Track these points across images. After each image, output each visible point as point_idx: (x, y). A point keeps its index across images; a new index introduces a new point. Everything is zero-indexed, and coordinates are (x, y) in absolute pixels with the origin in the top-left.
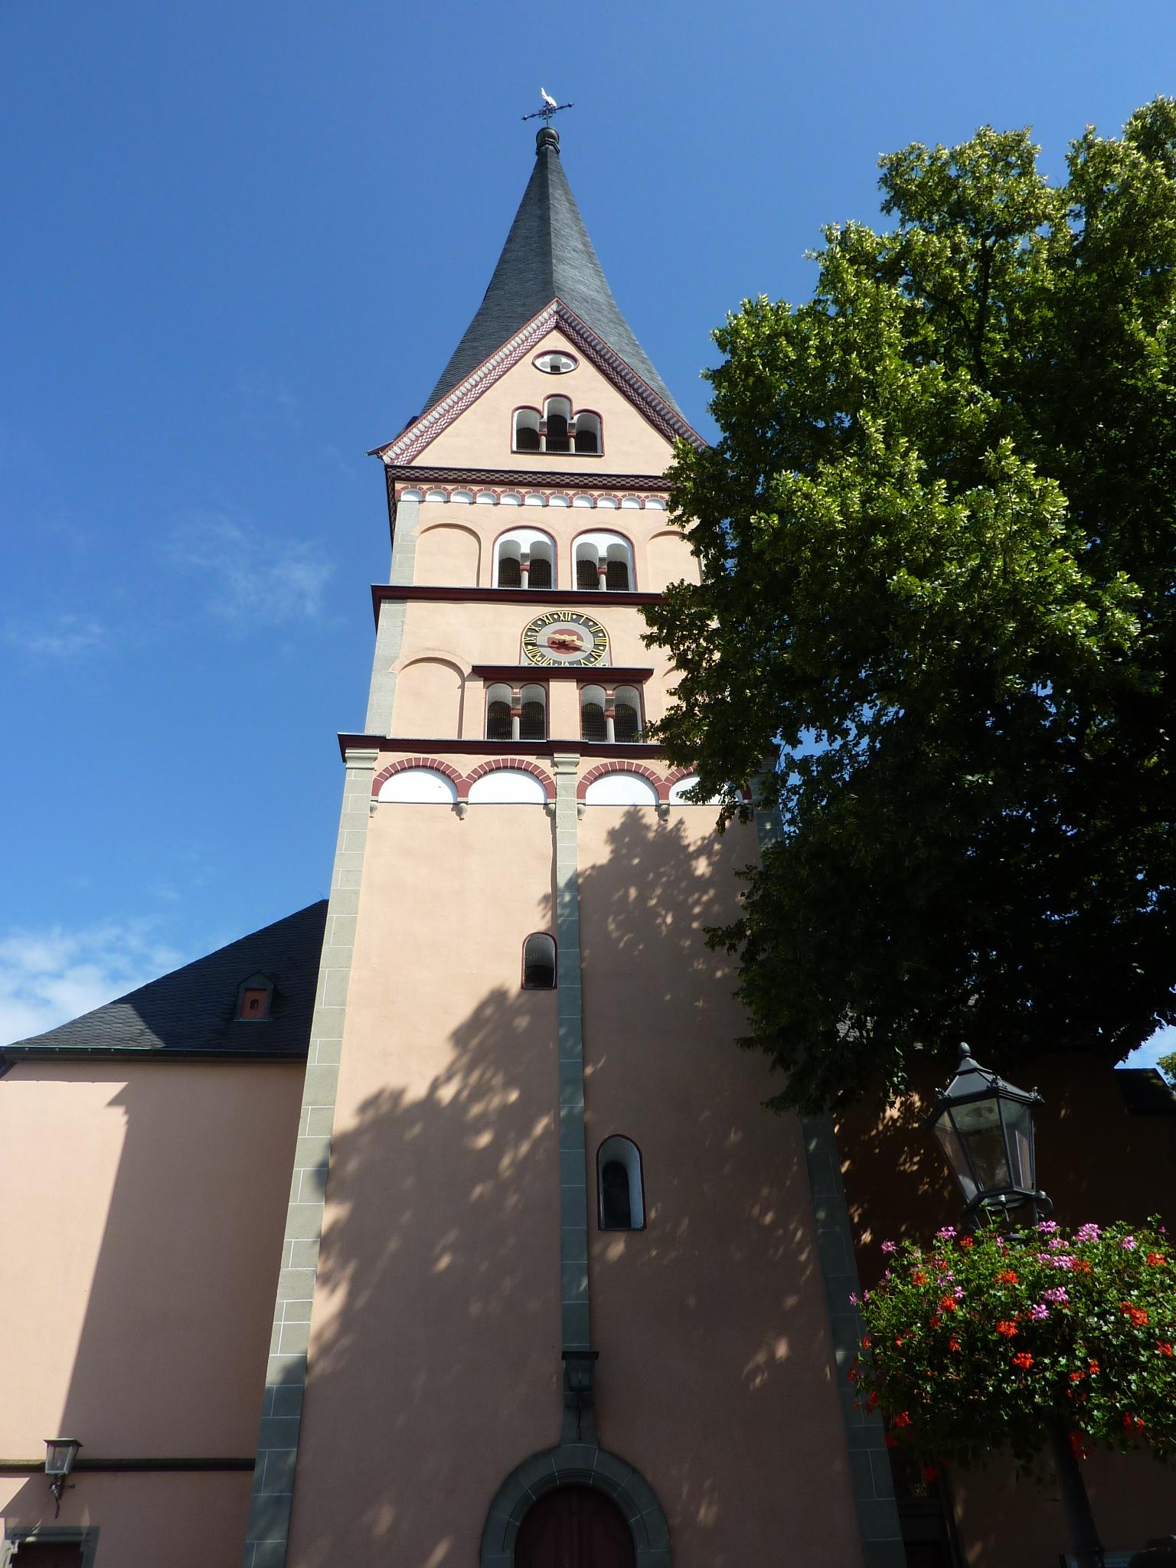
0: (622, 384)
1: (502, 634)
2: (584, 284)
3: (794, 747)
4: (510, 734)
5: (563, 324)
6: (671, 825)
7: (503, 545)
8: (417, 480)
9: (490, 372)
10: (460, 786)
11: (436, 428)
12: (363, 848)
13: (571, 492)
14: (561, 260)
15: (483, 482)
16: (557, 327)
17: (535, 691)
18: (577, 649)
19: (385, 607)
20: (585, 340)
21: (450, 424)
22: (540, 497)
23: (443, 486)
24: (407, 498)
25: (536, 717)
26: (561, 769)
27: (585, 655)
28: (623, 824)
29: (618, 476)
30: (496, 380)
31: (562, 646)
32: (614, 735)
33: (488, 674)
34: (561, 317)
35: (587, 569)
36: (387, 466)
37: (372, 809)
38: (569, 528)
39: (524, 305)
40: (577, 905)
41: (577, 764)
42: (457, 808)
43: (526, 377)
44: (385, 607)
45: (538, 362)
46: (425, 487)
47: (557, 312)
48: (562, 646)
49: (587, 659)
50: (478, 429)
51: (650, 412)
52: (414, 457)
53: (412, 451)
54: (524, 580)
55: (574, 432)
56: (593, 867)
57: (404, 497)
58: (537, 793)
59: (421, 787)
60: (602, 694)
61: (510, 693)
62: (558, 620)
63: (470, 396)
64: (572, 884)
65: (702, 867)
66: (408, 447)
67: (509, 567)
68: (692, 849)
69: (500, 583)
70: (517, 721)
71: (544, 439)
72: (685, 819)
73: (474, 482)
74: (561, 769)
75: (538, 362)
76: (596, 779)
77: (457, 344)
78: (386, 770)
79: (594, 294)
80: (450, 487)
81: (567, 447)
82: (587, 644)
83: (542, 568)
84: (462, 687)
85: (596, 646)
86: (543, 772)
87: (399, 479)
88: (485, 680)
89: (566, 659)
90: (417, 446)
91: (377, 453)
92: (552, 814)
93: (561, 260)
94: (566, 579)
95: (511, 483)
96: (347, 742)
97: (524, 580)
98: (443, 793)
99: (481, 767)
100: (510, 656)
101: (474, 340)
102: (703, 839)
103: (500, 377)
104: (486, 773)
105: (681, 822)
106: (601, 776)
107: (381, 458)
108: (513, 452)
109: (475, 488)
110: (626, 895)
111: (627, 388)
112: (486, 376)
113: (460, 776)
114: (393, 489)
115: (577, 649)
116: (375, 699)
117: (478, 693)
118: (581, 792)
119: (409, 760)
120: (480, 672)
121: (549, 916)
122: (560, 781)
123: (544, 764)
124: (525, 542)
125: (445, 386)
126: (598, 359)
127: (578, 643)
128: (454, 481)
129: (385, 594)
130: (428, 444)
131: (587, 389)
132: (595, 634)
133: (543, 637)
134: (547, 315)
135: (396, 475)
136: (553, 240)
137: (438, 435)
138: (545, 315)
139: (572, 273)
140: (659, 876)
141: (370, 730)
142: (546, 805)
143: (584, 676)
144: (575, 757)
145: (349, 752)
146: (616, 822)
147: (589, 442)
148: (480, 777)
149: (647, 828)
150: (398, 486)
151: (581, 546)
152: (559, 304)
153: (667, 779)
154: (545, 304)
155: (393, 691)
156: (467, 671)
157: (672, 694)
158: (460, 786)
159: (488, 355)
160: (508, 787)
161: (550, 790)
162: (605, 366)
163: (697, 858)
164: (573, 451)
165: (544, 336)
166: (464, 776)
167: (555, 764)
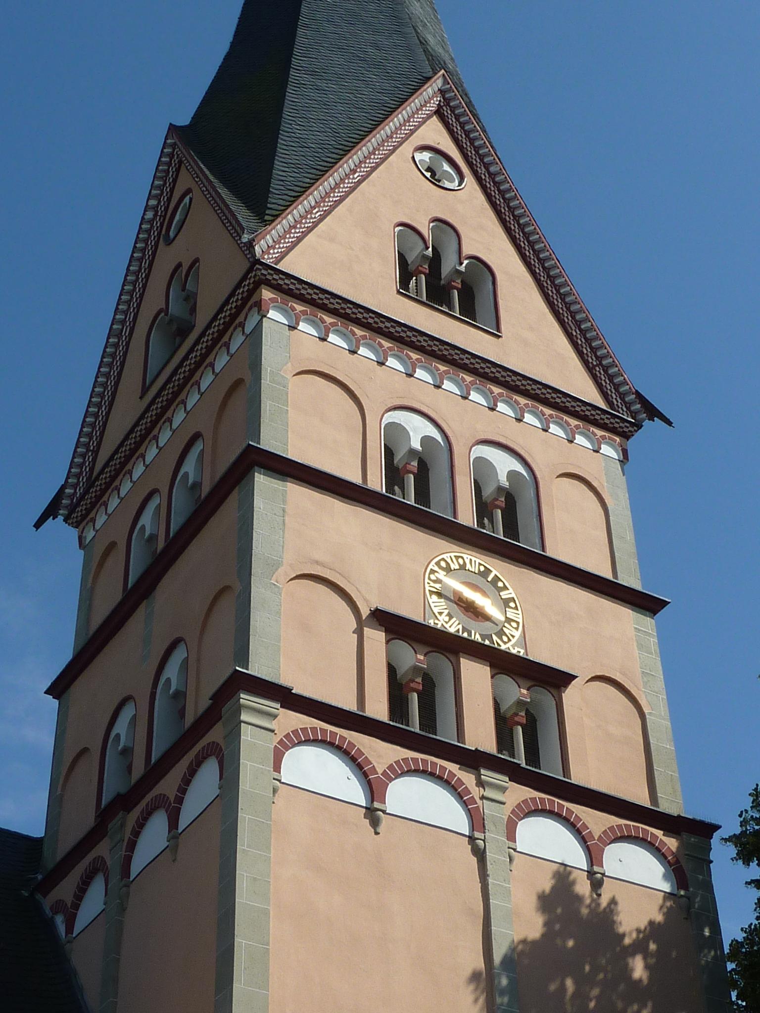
5: (447, 111)
6: (604, 901)
12: (268, 848)
15: (312, 303)
16: (438, 113)
17: (443, 663)
22: (284, 312)
23: (516, 397)
26: (489, 793)
31: (470, 609)
34: (447, 101)
40: (513, 989)
42: (373, 815)
45: (418, 156)
47: (442, 92)
56: (524, 941)
58: (460, 821)
64: (509, 961)
65: (638, 969)
68: (627, 941)
72: (619, 899)
74: (489, 793)
81: (450, 307)
88: (491, 666)
92: (480, 854)
98: (356, 794)
99: (304, 730)
102: (638, 931)
105: (613, 902)
110: (563, 988)
121: (482, 1000)
122: (488, 809)
123: (468, 779)
131: (484, 237)
140: (595, 969)
146: (546, 884)
149: (579, 899)
151: (390, 426)
152: (445, 82)
160: (417, 799)
161: (476, 820)
162: (499, 201)
163: (633, 955)
166: (380, 771)
167: (481, 784)
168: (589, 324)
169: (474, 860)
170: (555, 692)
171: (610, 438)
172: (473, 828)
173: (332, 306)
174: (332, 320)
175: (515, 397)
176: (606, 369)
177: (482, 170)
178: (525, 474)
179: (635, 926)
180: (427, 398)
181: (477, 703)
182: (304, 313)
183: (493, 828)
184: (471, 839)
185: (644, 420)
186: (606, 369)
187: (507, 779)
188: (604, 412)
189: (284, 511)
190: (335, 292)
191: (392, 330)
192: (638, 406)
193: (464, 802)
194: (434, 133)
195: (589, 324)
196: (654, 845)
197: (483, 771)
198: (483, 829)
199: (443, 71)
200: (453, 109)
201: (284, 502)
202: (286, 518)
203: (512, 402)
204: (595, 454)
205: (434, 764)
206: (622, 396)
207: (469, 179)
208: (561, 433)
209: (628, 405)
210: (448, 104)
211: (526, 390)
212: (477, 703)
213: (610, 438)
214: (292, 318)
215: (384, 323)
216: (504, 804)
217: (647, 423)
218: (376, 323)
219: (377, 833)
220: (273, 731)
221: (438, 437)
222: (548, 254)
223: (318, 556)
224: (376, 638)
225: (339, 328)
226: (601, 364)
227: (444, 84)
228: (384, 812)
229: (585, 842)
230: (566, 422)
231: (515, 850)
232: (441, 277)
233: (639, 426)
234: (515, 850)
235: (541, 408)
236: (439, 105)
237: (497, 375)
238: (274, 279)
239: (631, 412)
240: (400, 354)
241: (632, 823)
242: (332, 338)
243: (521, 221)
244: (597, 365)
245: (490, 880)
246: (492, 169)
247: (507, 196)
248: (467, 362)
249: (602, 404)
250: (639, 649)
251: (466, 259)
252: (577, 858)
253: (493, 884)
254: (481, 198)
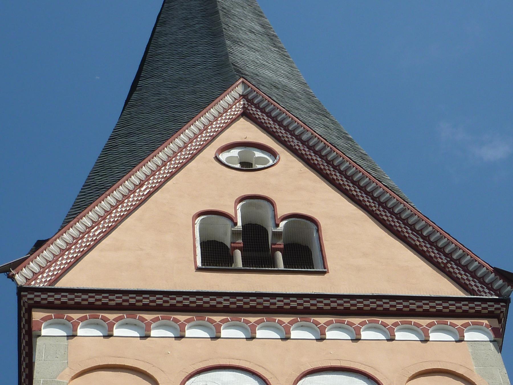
2: (269, 69)
9: (159, 168)
13: (286, 319)
14: (237, 42)
15: (158, 309)
16: (245, 114)
21: (106, 234)
22: (96, 325)
23: (102, 314)
24: (49, 332)
29: (366, 297)
30: (167, 179)
34: (250, 102)
36: (21, 289)
39: (194, 92)
43: (202, 178)
45: (223, 157)
46: (76, 316)
47: (243, 96)
51: (386, 216)
52: (59, 278)
55: (280, 244)
71: (238, 254)
73: (147, 308)
75: (223, 157)
79: (285, 81)
80: (111, 316)
81: (272, 262)
87: (39, 306)
91: (8, 270)
93: (237, 42)
95: (199, 310)
101: (129, 135)
103: (173, 175)
108: (198, 269)
109: (148, 317)
131: (294, 188)
134: (231, 98)
135: (33, 301)
136: (223, 19)
137: (90, 248)
139: (253, 56)
147: (302, 250)
150: (37, 315)
152: (246, 86)
154: (225, 87)
159: (153, 148)
164: (281, 267)
165: (228, 125)
168: (430, 229)
171: (474, 324)
175: (277, 318)
176: (457, 262)
182: (291, 323)
186: (457, 262)
188: (458, 300)
191: (186, 302)
192: (501, 282)
194: (245, 131)
199: (242, 80)
203: (99, 321)
206: (481, 280)
208: (412, 337)
209: (490, 287)
210: (253, 103)
213: (474, 324)
215: (174, 299)
218: (165, 302)
222: (374, 184)
225: (126, 320)
226: (452, 260)
227: (245, 89)
230: (416, 324)
232: (257, 241)
233: (507, 301)
235: (381, 320)
236: (243, 108)
237: (320, 305)
238: (43, 299)
240: (201, 322)
244: (448, 262)
246: (304, 137)
249: (459, 293)
251: (283, 219)
254: (298, 165)
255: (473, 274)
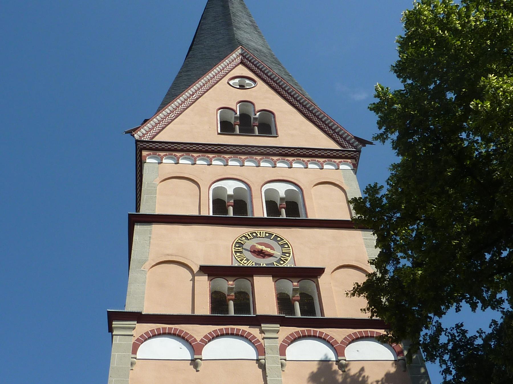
0: (286, 95)
1: (220, 245)
2: (254, 42)
3: (440, 317)
4: (227, 311)
7: (215, 190)
8: (157, 149)
9: (201, 87)
10: (195, 348)
11: (168, 119)
13: (259, 158)
14: (238, 29)
16: (242, 63)
17: (244, 283)
18: (270, 255)
19: (137, 228)
20: (261, 70)
21: (177, 117)
23: (287, 158)
25: (244, 301)
26: (267, 335)
27: (276, 259)
28: (319, 369)
30: (205, 92)
31: (261, 254)
32: (302, 313)
33: (211, 271)
34: (244, 57)
35: (272, 206)
36: (137, 141)
37: (132, 364)
38: (260, 180)
39: (218, 52)
41: (278, 331)
42: (194, 363)
43: (223, 91)
44: (137, 228)
45: (231, 82)
47: (241, 54)
48: (261, 254)
49: (278, 262)
50: (197, 119)
53: (153, 132)
54: (230, 212)
55: (257, 123)
57: (148, 161)
58: (250, 352)
59: (166, 349)
60: (290, 286)
61: (226, 285)
62: (257, 237)
63: (189, 101)
66: (150, 129)
67: (219, 204)
69: (214, 212)
70: (231, 303)
73: (195, 151)
74: (267, 335)
75: (231, 82)
76: (292, 342)
77: (177, 73)
78: (142, 336)
82: (277, 252)
83: (241, 204)
84: (193, 280)
85: (284, 253)
86: (254, 337)
87: (145, 149)
88: (208, 276)
89: (263, 262)
90: (156, 129)
91: (131, 132)
92: (263, 367)
93: (238, 29)
94: (260, 211)
96: (113, 316)
97: (230, 212)
98: (185, 353)
100: (225, 259)
101: (188, 71)
103: (208, 90)
104: (213, 338)
106: (295, 340)
107: (133, 136)
108: (219, 134)
109: (195, 155)
111: (289, 97)
112: (199, 89)
113: (195, 340)
114: (141, 155)
115: (270, 255)
116: (132, 288)
117: (204, 283)
118: (282, 352)
119: (158, 329)
120: (205, 270)
122: (267, 343)
123: (255, 331)
124: (230, 187)
125: (171, 95)
126: (269, 80)
127: (272, 252)
128: (181, 151)
129: (138, 219)
130: (163, 128)
132: (282, 246)
133: (248, 244)
134: (236, 55)
135: (142, 146)
138: (234, 55)
139: (246, 35)
141: (130, 307)
142: (258, 360)
143: (278, 273)
144: (276, 326)
145: (115, 324)
147: (267, 127)
148: (210, 341)
150: (144, 153)
151: (267, 191)
152: (242, 50)
153: (342, 342)
154: (232, 50)
155: (144, 282)
156: (196, 269)
157: (372, 263)
158: (195, 348)
160: (228, 348)
161: (260, 350)
162: (275, 85)
165: (234, 68)
166: (198, 340)
167: (262, 332)
168: (326, 118)
169: (260, 371)
170: (250, 279)
171: (344, 161)
172: (258, 354)
173: (179, 148)
174: (260, 157)
176: (338, 133)
177: (265, 76)
178: (296, 189)
179: (375, 380)
180: (228, 172)
181: (265, 295)
183: (270, 351)
184: (258, 360)
185: (361, 148)
187: (279, 326)
189: (150, 237)
190: (326, 148)
191: (213, 149)
193: (253, 343)
195: (326, 118)
196: (373, 337)
197: (262, 325)
198: (264, 353)
200: (247, 59)
201: (150, 233)
202: (151, 240)
203: (206, 158)
204: (258, 168)
205: (238, 330)
206: (348, 142)
207: (259, 82)
208: (316, 167)
209: (352, 145)
211: (316, 155)
212: (265, 295)
214: (174, 159)
216: (277, 338)
217: (363, 149)
219: (197, 371)
220: (132, 335)
221: (243, 186)
223: (168, 252)
224: (203, 281)
226: (335, 132)
228: (201, 359)
229: (333, 346)
231: (285, 360)
233: (360, 152)
234: (285, 360)
239: (354, 147)
241: (362, 330)
242: (310, 166)
243: (286, 89)
245: (268, 378)
246: (269, 74)
247: (278, 82)
248: (256, 151)
249: (339, 148)
250: (366, 247)
252: (332, 356)
253: (270, 380)
254: (266, 87)
255: (345, 139)
